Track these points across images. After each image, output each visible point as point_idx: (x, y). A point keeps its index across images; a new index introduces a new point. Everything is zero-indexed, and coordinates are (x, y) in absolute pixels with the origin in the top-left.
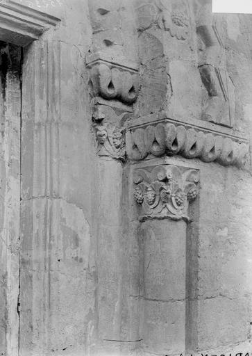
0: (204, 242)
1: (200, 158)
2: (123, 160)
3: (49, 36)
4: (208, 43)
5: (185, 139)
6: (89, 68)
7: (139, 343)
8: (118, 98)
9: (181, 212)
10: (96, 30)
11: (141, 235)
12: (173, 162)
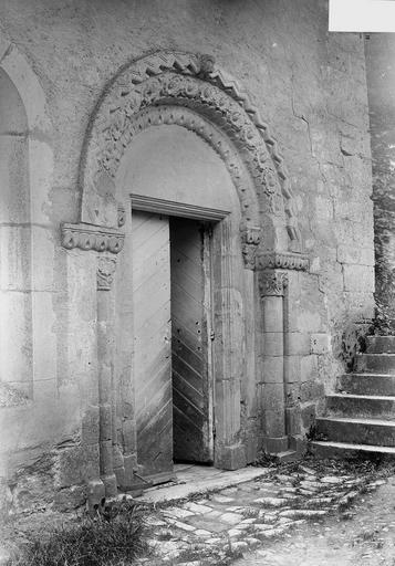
0: (290, 306)
1: (288, 268)
2: (254, 270)
3: (226, 219)
4: (290, 216)
5: (282, 261)
6: (40, 180)
7: (23, 395)
8: (253, 243)
9: (281, 293)
10: (243, 213)
11: (263, 304)
12: (278, 271)
